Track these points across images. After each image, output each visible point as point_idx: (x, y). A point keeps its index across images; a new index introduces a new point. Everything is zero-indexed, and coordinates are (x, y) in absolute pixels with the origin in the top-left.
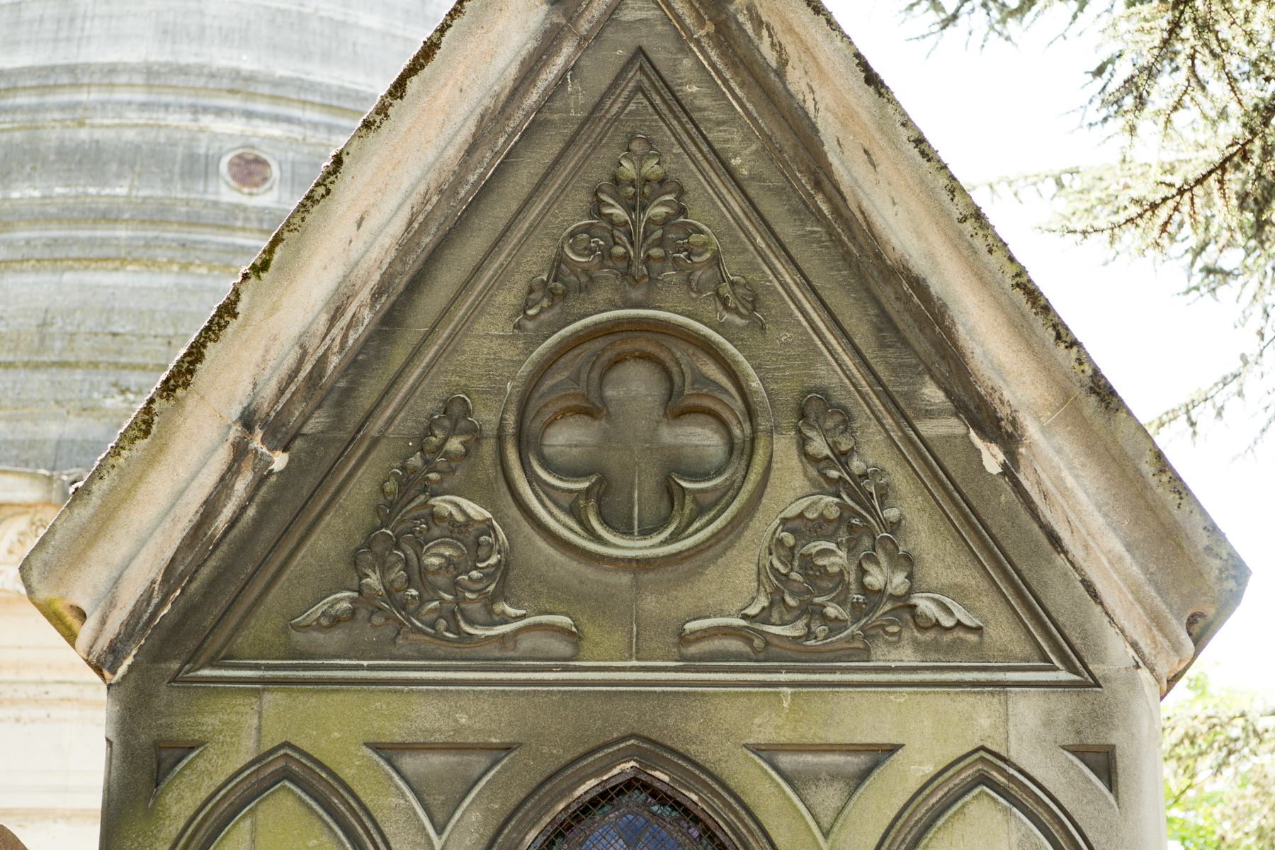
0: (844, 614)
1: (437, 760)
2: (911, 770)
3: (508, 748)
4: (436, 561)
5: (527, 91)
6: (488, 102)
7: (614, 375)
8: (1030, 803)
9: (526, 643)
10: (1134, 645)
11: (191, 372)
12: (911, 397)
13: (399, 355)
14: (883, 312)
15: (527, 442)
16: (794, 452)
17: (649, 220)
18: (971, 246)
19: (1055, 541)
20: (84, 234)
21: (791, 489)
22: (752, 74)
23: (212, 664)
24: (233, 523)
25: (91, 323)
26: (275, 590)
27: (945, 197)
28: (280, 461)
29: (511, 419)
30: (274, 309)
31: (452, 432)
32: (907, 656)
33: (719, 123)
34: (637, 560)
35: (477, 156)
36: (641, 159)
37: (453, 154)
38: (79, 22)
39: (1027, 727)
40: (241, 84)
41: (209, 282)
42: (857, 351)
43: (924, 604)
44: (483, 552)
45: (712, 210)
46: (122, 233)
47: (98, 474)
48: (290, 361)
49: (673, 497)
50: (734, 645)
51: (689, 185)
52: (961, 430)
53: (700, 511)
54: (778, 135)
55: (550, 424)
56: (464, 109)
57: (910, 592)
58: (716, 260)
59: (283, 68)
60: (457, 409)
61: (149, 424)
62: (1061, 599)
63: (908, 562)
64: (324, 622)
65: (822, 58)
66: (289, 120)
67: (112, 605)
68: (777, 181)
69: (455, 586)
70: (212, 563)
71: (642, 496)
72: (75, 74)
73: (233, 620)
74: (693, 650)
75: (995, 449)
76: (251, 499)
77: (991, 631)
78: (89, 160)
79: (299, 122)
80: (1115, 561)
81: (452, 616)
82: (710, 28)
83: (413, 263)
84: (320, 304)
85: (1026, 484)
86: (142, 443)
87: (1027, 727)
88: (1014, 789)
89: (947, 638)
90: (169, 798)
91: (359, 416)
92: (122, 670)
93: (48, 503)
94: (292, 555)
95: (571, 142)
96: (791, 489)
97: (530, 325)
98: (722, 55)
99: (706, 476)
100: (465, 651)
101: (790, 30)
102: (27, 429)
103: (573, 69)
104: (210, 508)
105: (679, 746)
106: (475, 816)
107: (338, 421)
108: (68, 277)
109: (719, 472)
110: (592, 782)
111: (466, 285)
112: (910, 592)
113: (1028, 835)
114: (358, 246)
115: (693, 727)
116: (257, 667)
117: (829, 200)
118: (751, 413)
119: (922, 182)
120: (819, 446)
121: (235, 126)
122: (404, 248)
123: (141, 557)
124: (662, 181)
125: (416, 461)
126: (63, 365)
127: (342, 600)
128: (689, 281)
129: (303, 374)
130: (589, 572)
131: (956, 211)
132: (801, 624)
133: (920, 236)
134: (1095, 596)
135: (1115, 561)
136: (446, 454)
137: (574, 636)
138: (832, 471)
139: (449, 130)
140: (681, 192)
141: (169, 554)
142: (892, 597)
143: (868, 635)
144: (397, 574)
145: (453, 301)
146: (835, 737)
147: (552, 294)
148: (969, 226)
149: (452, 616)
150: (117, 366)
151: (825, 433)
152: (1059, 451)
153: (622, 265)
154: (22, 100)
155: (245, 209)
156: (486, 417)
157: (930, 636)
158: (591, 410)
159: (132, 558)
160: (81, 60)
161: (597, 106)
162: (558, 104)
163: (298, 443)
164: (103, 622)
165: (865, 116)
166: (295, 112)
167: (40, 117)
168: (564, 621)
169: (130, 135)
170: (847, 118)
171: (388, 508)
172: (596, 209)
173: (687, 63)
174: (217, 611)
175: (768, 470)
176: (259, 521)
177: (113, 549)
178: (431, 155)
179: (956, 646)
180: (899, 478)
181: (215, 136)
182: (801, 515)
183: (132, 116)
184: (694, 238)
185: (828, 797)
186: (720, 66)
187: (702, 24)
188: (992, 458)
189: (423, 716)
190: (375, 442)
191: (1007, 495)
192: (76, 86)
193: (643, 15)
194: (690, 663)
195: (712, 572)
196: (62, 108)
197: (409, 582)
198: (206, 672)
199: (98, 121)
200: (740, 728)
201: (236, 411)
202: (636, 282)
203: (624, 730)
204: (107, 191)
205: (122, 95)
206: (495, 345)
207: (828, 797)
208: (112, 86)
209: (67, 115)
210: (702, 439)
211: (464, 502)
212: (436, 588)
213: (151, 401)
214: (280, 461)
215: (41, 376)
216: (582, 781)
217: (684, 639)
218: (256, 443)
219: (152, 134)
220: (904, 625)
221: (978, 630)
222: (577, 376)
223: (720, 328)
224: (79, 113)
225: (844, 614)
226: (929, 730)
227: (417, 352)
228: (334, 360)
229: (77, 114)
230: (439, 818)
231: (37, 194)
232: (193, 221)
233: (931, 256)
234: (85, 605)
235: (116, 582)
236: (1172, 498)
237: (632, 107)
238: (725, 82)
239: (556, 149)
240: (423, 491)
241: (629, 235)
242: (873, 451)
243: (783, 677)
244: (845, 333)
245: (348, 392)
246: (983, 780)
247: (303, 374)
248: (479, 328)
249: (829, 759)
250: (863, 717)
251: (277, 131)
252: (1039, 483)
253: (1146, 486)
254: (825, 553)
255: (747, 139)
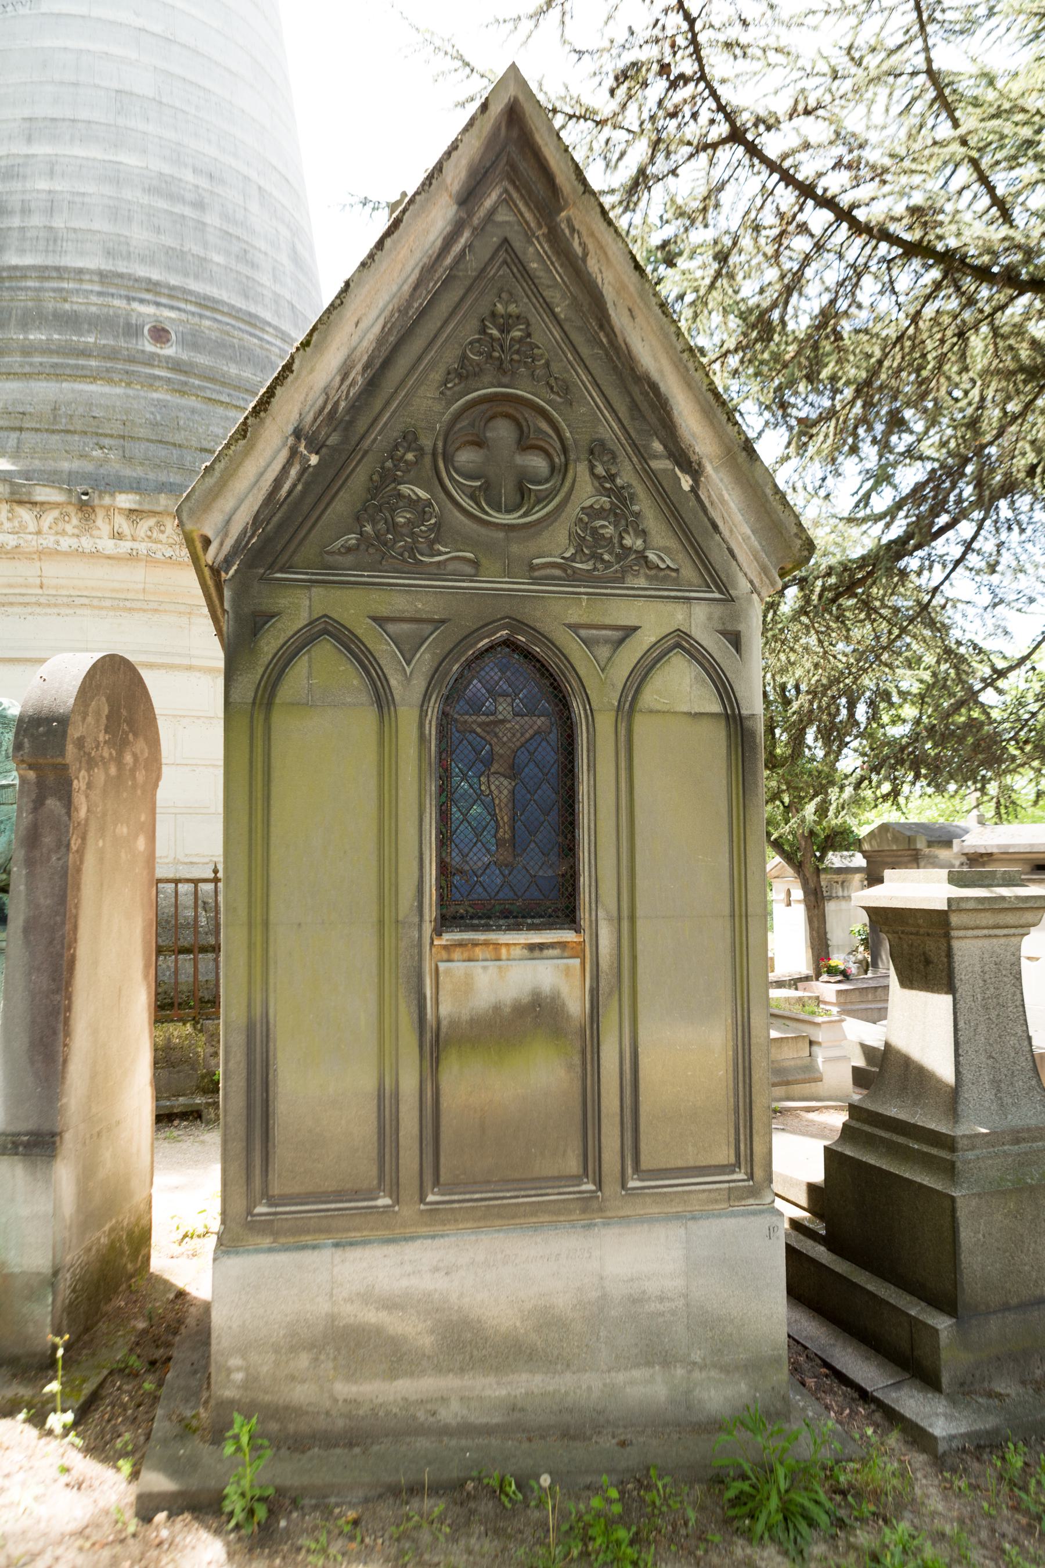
0: (612, 560)
1: (406, 626)
2: (646, 638)
3: (443, 622)
4: (402, 520)
5: (445, 257)
6: (425, 260)
7: (490, 424)
8: (700, 657)
9: (451, 567)
10: (751, 582)
11: (268, 403)
12: (647, 447)
13: (378, 404)
14: (633, 401)
15: (448, 459)
16: (587, 473)
17: (512, 339)
18: (686, 366)
19: (715, 527)
20: (72, 362)
21: (585, 493)
22: (568, 258)
23: (281, 571)
24: (290, 493)
25: (81, 410)
26: (314, 532)
27: (674, 338)
28: (314, 460)
29: (440, 444)
30: (312, 370)
31: (409, 449)
32: (642, 582)
33: (549, 287)
34: (508, 525)
35: (418, 292)
36: (506, 305)
37: (407, 288)
38: (59, 242)
39: (699, 620)
40: (153, 287)
41: (142, 393)
42: (620, 421)
43: (652, 556)
44: (427, 517)
45: (546, 336)
46: (93, 363)
47: (218, 459)
48: (320, 402)
49: (523, 494)
50: (557, 572)
51: (532, 321)
52: (671, 467)
53: (538, 501)
54: (580, 297)
55: (457, 449)
56: (412, 263)
57: (645, 549)
58: (547, 365)
59: (174, 280)
60: (410, 437)
61: (245, 431)
62: (718, 557)
63: (643, 533)
64: (343, 550)
65: (610, 253)
66: (179, 309)
67: (226, 535)
68: (579, 323)
69: (412, 534)
70: (279, 515)
71: (507, 491)
72: (60, 272)
73: (292, 547)
74: (536, 574)
75: (688, 478)
76: (299, 480)
77: (683, 571)
78: (71, 321)
79: (184, 311)
80: (746, 539)
81: (412, 550)
82: (545, 230)
83: (384, 353)
84: (335, 371)
85: (703, 497)
86: (242, 442)
87: (699, 620)
88: (693, 650)
89: (662, 574)
90: (262, 643)
91: (357, 438)
92: (232, 572)
93: (70, 503)
94: (326, 509)
95: (469, 290)
96: (585, 493)
97: (448, 393)
98: (551, 247)
99: (540, 483)
100: (418, 569)
101: (592, 234)
102: (51, 465)
103: (469, 246)
104: (278, 483)
105: (531, 624)
106: (427, 656)
107: (345, 439)
108: (65, 385)
109: (547, 481)
110: (486, 641)
111: (413, 367)
112: (645, 549)
113: (699, 674)
114: (355, 339)
115: (538, 614)
116: (307, 574)
117: (607, 336)
118: (565, 450)
119: (662, 328)
120: (600, 470)
121: (151, 310)
122: (380, 341)
123: (242, 508)
124: (518, 317)
125: (389, 464)
126: (68, 432)
127: (352, 539)
128: (533, 375)
129: (326, 411)
130: (483, 530)
131: (680, 347)
132: (591, 563)
133: (656, 359)
134: (733, 556)
135: (746, 539)
136: (406, 462)
137: (475, 563)
138: (606, 483)
139: (404, 275)
140: (528, 325)
141: (256, 508)
142: (636, 551)
143: (624, 571)
144: (381, 526)
145: (407, 375)
146: (608, 621)
147: (460, 376)
148: (686, 355)
149: (412, 550)
150: (97, 434)
151: (603, 463)
152: (721, 480)
153: (497, 363)
154: (30, 284)
155: (159, 356)
156: (427, 442)
157: (653, 572)
158: (479, 443)
159: (236, 510)
160: (62, 264)
161: (483, 270)
162: (462, 266)
163: (324, 450)
164: (221, 544)
165: (632, 289)
166: (182, 305)
167: (41, 294)
168: (471, 555)
169: (93, 309)
170: (621, 289)
171: (374, 490)
172: (483, 330)
173: (531, 250)
174: (283, 542)
175: (574, 481)
176: (304, 493)
177: (226, 503)
178: (394, 288)
179: (666, 578)
180: (639, 490)
181: (140, 314)
182: (591, 506)
183: (94, 299)
184: (536, 351)
185: (604, 652)
186: (549, 253)
187: (540, 227)
188: (686, 483)
189: (399, 603)
190: (366, 452)
191: (693, 502)
192: (61, 278)
193: (507, 218)
194: (536, 581)
195: (546, 534)
196: (54, 290)
197: (388, 532)
198: (279, 575)
199: (75, 299)
200: (563, 616)
201: (290, 429)
202: (505, 373)
203: (503, 614)
204: (83, 339)
205: (87, 286)
206: (430, 402)
207: (604, 652)
208: (81, 281)
209: (57, 295)
210: (537, 463)
211: (416, 489)
212: (403, 535)
213: (246, 418)
214: (314, 460)
215: (56, 437)
216: (482, 640)
217: (532, 568)
218: (302, 448)
219: (105, 310)
220: (641, 566)
221: (677, 570)
222: (471, 427)
223: (548, 402)
224: (64, 294)
225: (612, 560)
226: (653, 619)
227: (388, 403)
228: (343, 404)
229: (64, 295)
230: (408, 656)
231: (44, 337)
232: (131, 360)
233: (661, 371)
234: (210, 534)
235: (228, 522)
236: (780, 507)
237: (501, 273)
238: (552, 263)
239: (461, 292)
240: (394, 481)
241: (502, 347)
242: (626, 476)
243: (582, 590)
244: (614, 411)
245: (351, 423)
246: (678, 645)
247: (326, 411)
248: (421, 392)
249: (604, 632)
250: (623, 613)
251: (173, 314)
252: (709, 497)
253: (767, 501)
254: (603, 527)
255: (564, 297)
